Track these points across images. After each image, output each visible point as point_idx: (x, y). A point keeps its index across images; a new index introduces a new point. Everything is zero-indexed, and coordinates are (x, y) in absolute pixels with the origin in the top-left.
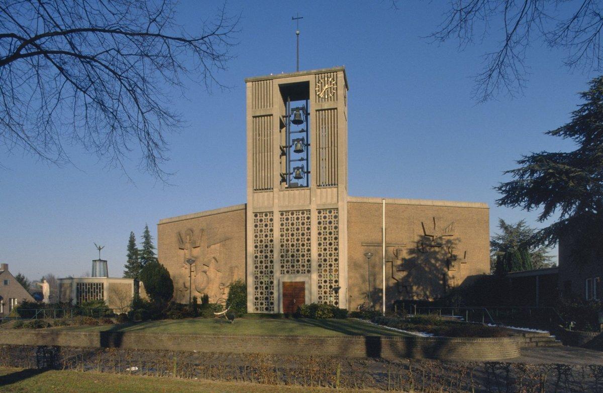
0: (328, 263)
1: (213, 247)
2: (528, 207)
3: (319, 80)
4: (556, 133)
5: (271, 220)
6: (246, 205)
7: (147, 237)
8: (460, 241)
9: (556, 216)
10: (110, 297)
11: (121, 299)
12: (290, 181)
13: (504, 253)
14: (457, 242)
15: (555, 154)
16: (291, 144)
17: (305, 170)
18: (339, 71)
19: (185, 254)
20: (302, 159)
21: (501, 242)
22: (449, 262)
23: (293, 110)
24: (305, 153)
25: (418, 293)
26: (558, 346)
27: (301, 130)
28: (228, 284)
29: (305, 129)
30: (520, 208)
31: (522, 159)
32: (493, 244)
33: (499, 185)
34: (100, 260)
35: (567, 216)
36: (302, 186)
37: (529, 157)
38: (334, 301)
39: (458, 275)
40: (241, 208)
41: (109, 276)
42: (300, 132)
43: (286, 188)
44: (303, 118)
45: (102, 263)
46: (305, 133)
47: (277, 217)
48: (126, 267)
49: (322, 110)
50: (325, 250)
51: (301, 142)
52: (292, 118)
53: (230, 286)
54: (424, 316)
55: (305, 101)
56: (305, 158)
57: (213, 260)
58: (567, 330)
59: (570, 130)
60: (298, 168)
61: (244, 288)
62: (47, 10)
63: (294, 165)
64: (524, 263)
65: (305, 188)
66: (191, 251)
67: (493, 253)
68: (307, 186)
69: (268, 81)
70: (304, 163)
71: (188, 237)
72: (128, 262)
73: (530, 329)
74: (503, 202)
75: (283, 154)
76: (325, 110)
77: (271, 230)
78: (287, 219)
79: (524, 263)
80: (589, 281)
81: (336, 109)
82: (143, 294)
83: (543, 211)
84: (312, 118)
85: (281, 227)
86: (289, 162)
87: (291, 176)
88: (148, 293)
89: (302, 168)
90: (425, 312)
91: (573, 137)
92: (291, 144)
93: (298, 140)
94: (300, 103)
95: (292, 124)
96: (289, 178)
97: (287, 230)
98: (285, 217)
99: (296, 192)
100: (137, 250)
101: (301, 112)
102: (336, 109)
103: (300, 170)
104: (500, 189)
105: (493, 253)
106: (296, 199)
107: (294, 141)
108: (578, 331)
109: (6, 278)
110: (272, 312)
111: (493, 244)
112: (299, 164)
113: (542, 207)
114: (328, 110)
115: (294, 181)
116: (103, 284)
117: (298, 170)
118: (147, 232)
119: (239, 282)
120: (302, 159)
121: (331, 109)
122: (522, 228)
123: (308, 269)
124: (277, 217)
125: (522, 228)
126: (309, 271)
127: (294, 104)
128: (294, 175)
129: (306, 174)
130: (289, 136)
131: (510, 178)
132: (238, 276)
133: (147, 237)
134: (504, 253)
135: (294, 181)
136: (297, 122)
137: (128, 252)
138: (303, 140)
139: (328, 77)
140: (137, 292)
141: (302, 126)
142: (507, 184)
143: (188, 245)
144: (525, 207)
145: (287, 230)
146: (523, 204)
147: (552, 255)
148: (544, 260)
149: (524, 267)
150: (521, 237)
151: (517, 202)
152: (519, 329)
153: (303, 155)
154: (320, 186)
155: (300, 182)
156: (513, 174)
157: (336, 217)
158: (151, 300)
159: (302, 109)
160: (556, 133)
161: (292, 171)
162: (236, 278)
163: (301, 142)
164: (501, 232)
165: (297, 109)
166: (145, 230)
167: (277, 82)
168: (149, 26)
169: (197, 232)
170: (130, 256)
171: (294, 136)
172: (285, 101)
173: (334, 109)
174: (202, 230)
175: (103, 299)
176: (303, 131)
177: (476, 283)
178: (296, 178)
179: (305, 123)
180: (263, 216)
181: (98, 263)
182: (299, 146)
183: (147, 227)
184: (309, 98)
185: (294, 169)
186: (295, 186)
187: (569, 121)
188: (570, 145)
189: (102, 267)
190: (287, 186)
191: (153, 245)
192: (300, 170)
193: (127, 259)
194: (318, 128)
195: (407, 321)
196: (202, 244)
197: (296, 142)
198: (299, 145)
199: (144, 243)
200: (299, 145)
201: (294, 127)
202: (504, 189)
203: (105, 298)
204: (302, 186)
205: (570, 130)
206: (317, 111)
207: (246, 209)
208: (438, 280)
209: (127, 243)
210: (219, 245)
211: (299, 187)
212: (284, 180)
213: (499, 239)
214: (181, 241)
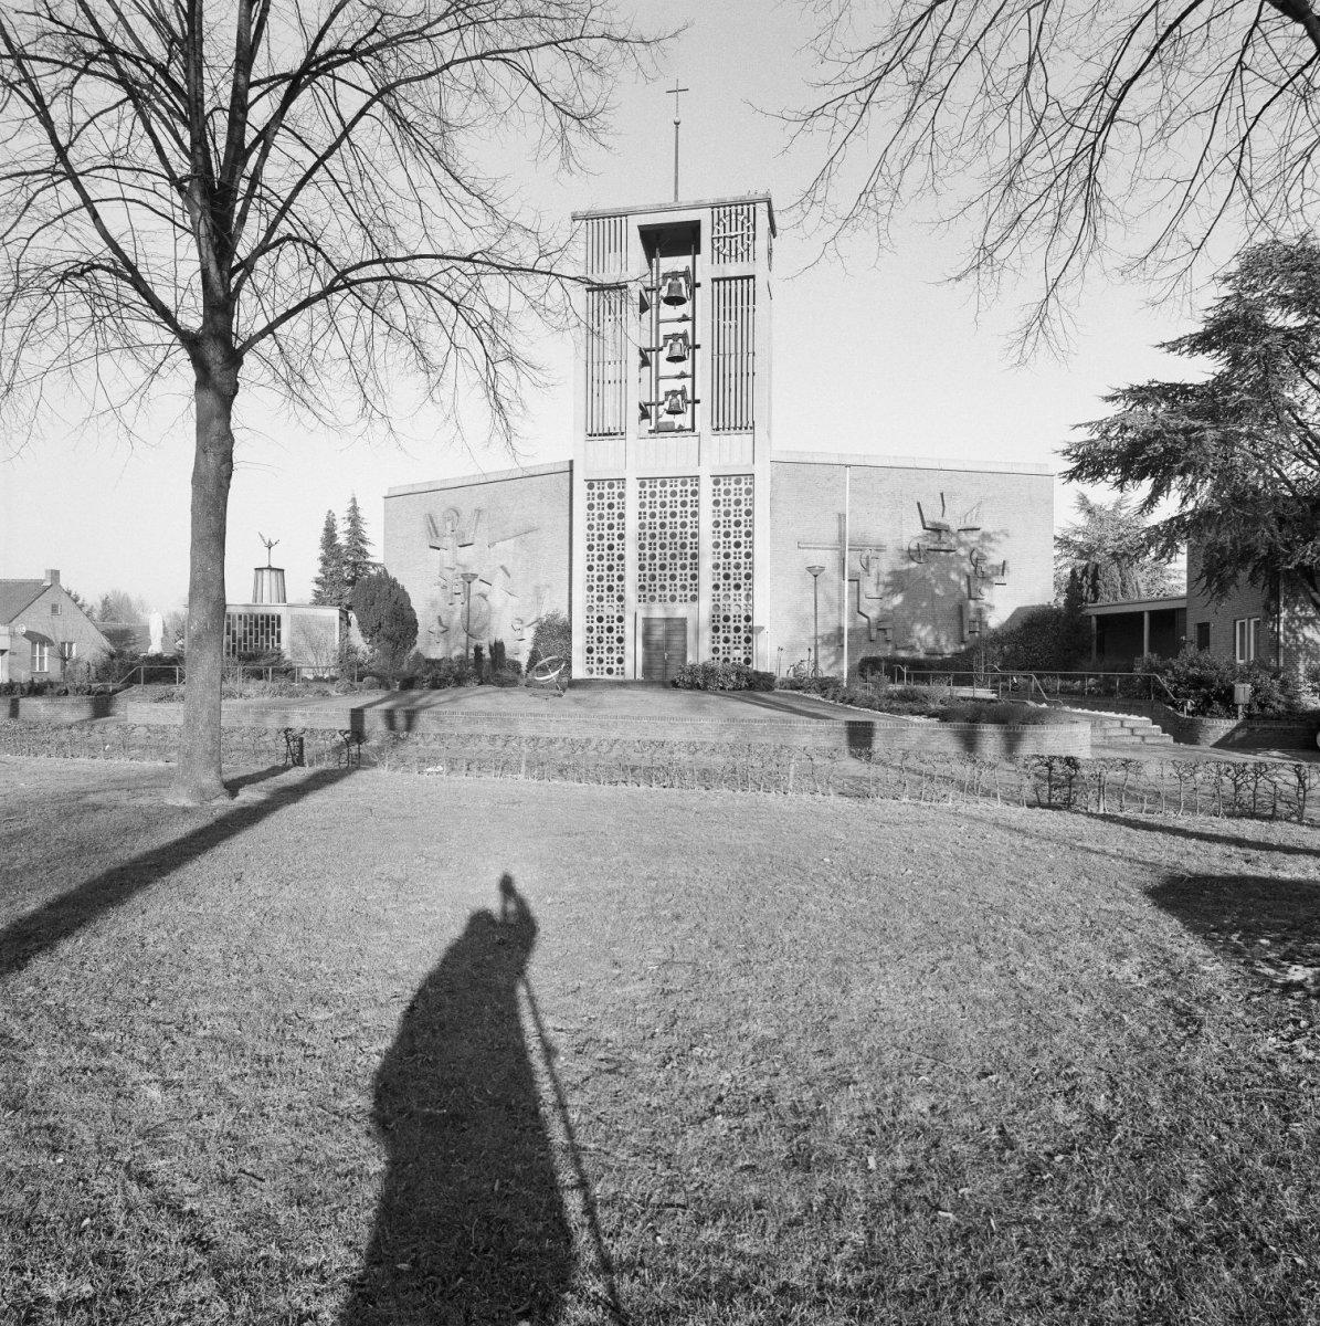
0: (737, 576)
1: (499, 545)
2: (1120, 484)
3: (719, 220)
4: (1174, 346)
5: (621, 495)
6: (571, 462)
7: (354, 519)
8: (1007, 535)
9: (1170, 506)
10: (293, 644)
11: (316, 648)
12: (658, 417)
13: (1085, 563)
14: (1001, 537)
15: (1173, 386)
16: (661, 344)
17: (689, 397)
18: (760, 201)
19: (442, 561)
20: (683, 376)
21: (1080, 538)
22: (982, 574)
23: (666, 276)
24: (688, 362)
25: (925, 638)
26: (1164, 745)
27: (680, 316)
28: (533, 619)
29: (690, 316)
30: (1107, 486)
31: (1111, 393)
32: (1064, 543)
33: (1065, 447)
34: (270, 568)
35: (1191, 505)
36: (681, 429)
37: (1124, 391)
38: (743, 657)
39: (1001, 606)
40: (559, 469)
41: (288, 601)
42: (680, 320)
43: (651, 432)
44: (684, 293)
45: (273, 574)
46: (690, 323)
47: (632, 489)
48: (318, 582)
49: (724, 279)
50: (727, 556)
51: (681, 341)
52: (664, 292)
53: (536, 625)
54: (923, 688)
55: (690, 258)
56: (689, 372)
57: (501, 573)
58: (1180, 715)
59: (1202, 343)
60: (674, 393)
61: (566, 631)
62: (129, 19)
63: (666, 386)
64: (1124, 585)
65: (688, 433)
66: (455, 553)
67: (1064, 561)
68: (693, 429)
69: (618, 219)
70: (687, 382)
71: (449, 525)
72: (322, 571)
73: (1117, 713)
74: (1073, 475)
75: (645, 363)
76: (730, 279)
77: (621, 516)
78: (653, 494)
79: (1124, 585)
80: (1242, 625)
81: (753, 277)
82: (358, 640)
83: (1149, 492)
84: (703, 295)
85: (639, 489)
86: (657, 381)
87: (661, 408)
88: (364, 633)
89: (683, 392)
90: (924, 679)
91: (1208, 354)
92: (661, 344)
93: (675, 337)
94: (680, 263)
95: (663, 304)
96: (657, 412)
97: (653, 515)
98: (648, 490)
99: (669, 442)
100: (339, 548)
101: (682, 280)
102: (753, 277)
103: (679, 397)
104: (1067, 452)
105: (1064, 561)
106: (671, 456)
107: (666, 338)
108: (1199, 717)
109: (54, 600)
110: (620, 678)
111: (1064, 543)
112: (677, 385)
113: (1147, 485)
114: (736, 278)
115: (667, 418)
116: (279, 617)
117: (675, 396)
118: (354, 509)
119: (555, 617)
120: (683, 376)
121: (742, 278)
122: (1124, 512)
123: (695, 509)
124: (632, 489)
125: (1124, 512)
126: (694, 598)
127: (669, 264)
128: (667, 405)
129: (689, 406)
130: (657, 384)
131: (1083, 435)
132: (554, 605)
133: (354, 519)
134: (1085, 563)
135: (667, 418)
136: (674, 301)
137: (323, 551)
138: (684, 336)
139: (737, 214)
140: (345, 636)
141: (685, 309)
142: (1079, 445)
143: (448, 541)
144: (1116, 484)
145: (653, 515)
146: (1111, 478)
147: (1175, 574)
148: (1170, 577)
149: (1124, 592)
150: (1121, 530)
151: (1101, 475)
152: (1096, 712)
153: (685, 366)
154: (718, 429)
155: (678, 420)
156: (1089, 429)
157: (748, 492)
158: (372, 651)
159: (685, 274)
160: (1174, 346)
161: (662, 398)
162: (544, 612)
163: (681, 341)
164: (1081, 520)
165: (675, 275)
166: (351, 505)
167: (635, 222)
168: (333, 16)
169: (467, 513)
170: (325, 562)
171: (666, 329)
172: (650, 254)
173: (748, 278)
174: (479, 511)
175: (279, 649)
176: (684, 319)
177: (1033, 624)
178: (669, 412)
179: (689, 304)
180: (606, 489)
181: (266, 573)
182: (677, 351)
183: (354, 500)
184: (698, 251)
185: (667, 394)
186: (669, 429)
187: (1200, 328)
188: (1201, 369)
189: (274, 580)
190: (652, 428)
191: (367, 536)
192: (679, 397)
193: (320, 565)
194: (717, 313)
195: (890, 697)
196: (478, 540)
197: (671, 341)
198: (677, 348)
199: (348, 532)
200: (677, 348)
201: (668, 311)
202: (1074, 453)
203: (284, 646)
204: (681, 429)
205: (1202, 343)
206: (713, 280)
207: (571, 471)
208: (962, 615)
209: (321, 533)
210: (512, 541)
211: (677, 431)
212: (645, 415)
213: (1076, 532)
214: (434, 531)
